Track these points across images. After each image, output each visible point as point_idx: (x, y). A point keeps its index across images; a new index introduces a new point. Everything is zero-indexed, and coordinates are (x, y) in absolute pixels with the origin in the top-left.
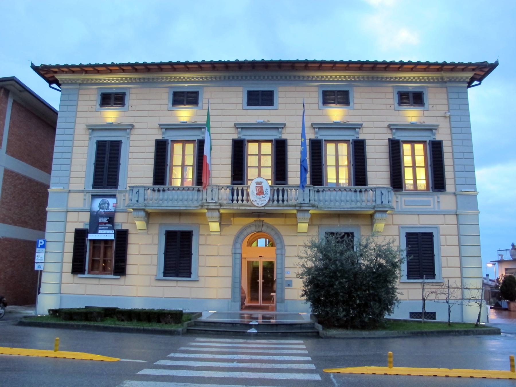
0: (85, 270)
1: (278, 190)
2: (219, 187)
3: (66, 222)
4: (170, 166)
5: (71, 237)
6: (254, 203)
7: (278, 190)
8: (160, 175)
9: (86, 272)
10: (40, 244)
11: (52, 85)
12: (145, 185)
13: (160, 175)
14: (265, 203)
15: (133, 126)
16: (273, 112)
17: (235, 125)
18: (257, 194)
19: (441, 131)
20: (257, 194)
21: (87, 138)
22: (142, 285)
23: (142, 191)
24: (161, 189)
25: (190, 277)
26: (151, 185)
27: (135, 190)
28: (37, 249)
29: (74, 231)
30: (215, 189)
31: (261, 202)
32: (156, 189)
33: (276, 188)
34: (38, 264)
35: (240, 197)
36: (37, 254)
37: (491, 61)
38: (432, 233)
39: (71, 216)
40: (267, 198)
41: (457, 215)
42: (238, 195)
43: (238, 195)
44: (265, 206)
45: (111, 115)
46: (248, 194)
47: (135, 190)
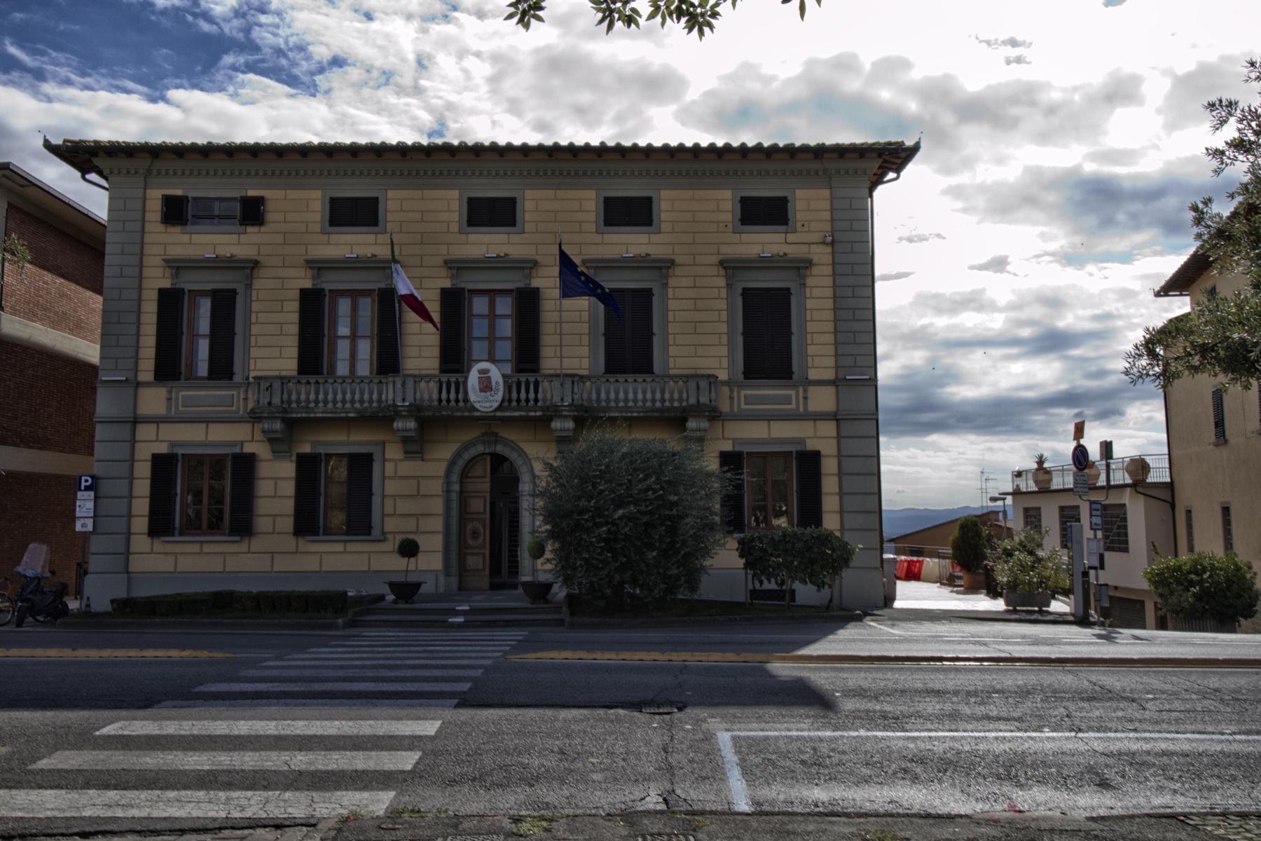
0: (174, 528)
1: (449, 384)
2: (418, 378)
3: (133, 441)
4: (329, 338)
5: (144, 470)
6: (477, 405)
7: (449, 384)
8: (388, 360)
9: (177, 532)
10: (83, 484)
11: (88, 176)
12: (283, 373)
13: (313, 357)
14: (496, 405)
15: (672, 262)
16: (515, 238)
17: (446, 262)
18: (481, 390)
19: (542, 271)
20: (481, 390)
21: (722, 282)
22: (274, 555)
23: (277, 385)
24: (312, 381)
25: (369, 534)
26: (437, 372)
27: (264, 385)
28: (80, 494)
29: (150, 458)
30: (410, 384)
31: (488, 405)
32: (304, 381)
33: (444, 380)
34: (82, 521)
35: (453, 396)
36: (78, 503)
37: (909, 143)
38: (371, 454)
39: (145, 432)
40: (499, 396)
41: (837, 420)
42: (527, 392)
43: (527, 392)
44: (495, 410)
45: (764, 242)
46: (466, 392)
47: (264, 385)
